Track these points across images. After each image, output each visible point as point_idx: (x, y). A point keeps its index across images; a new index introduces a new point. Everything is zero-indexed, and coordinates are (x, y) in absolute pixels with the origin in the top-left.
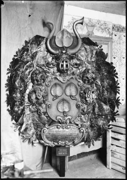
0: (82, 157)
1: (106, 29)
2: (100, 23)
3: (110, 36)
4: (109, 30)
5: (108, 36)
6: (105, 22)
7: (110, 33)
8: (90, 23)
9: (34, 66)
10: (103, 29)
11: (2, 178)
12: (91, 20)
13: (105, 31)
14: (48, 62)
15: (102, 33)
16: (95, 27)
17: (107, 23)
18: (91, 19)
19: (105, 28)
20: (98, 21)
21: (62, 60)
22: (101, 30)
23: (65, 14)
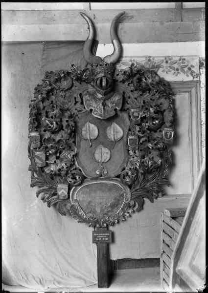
0: (142, 267)
1: (186, 69)
2: (170, 60)
3: (194, 78)
4: (192, 69)
5: (190, 78)
6: (183, 58)
7: (194, 74)
8: (149, 63)
9: (45, 114)
10: (177, 70)
11: (202, 5)
12: (151, 59)
13: (182, 71)
14: (158, 279)
15: (177, 75)
16: (160, 69)
17: (186, 58)
18: (150, 57)
19: (182, 68)
20: (166, 58)
21: (84, 197)
22: (173, 72)
23: (108, 20)
